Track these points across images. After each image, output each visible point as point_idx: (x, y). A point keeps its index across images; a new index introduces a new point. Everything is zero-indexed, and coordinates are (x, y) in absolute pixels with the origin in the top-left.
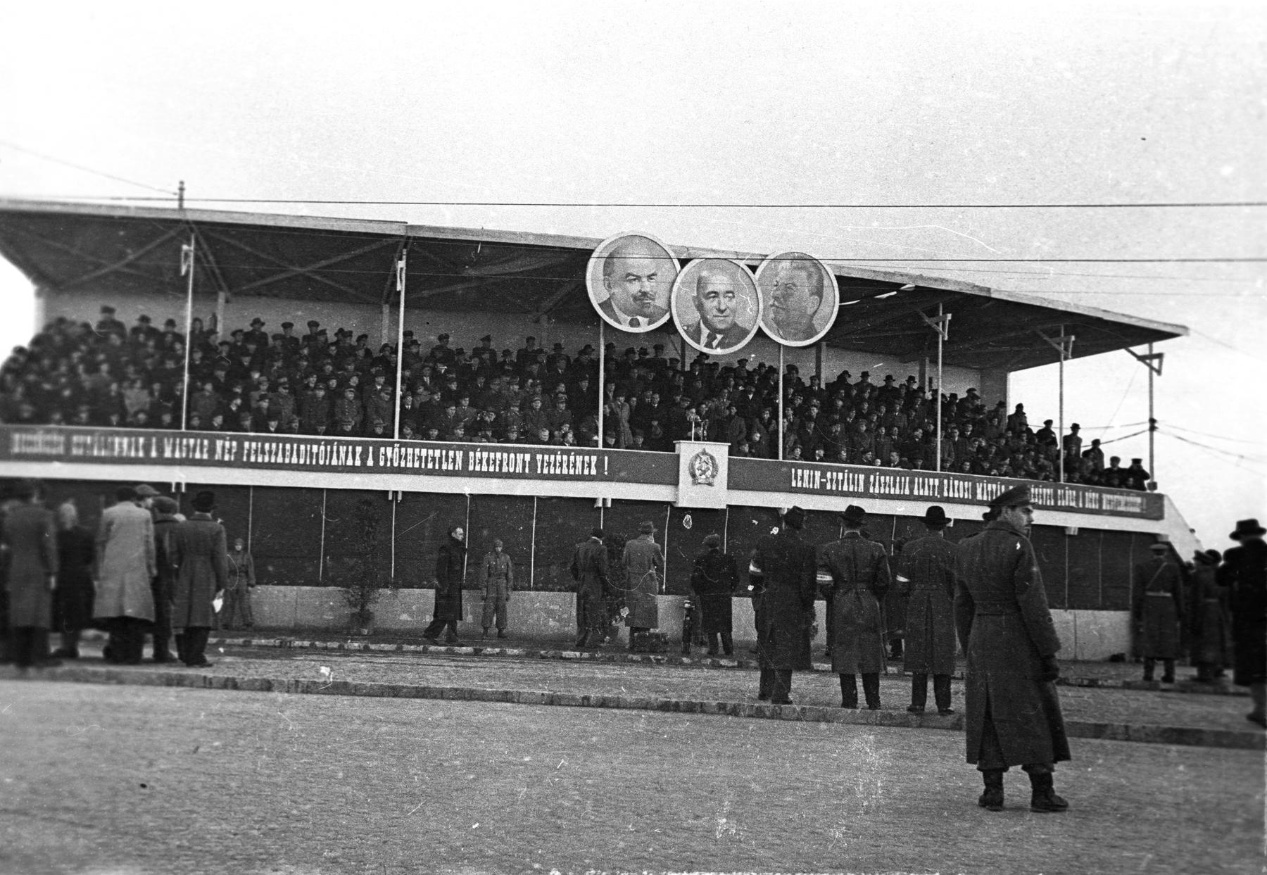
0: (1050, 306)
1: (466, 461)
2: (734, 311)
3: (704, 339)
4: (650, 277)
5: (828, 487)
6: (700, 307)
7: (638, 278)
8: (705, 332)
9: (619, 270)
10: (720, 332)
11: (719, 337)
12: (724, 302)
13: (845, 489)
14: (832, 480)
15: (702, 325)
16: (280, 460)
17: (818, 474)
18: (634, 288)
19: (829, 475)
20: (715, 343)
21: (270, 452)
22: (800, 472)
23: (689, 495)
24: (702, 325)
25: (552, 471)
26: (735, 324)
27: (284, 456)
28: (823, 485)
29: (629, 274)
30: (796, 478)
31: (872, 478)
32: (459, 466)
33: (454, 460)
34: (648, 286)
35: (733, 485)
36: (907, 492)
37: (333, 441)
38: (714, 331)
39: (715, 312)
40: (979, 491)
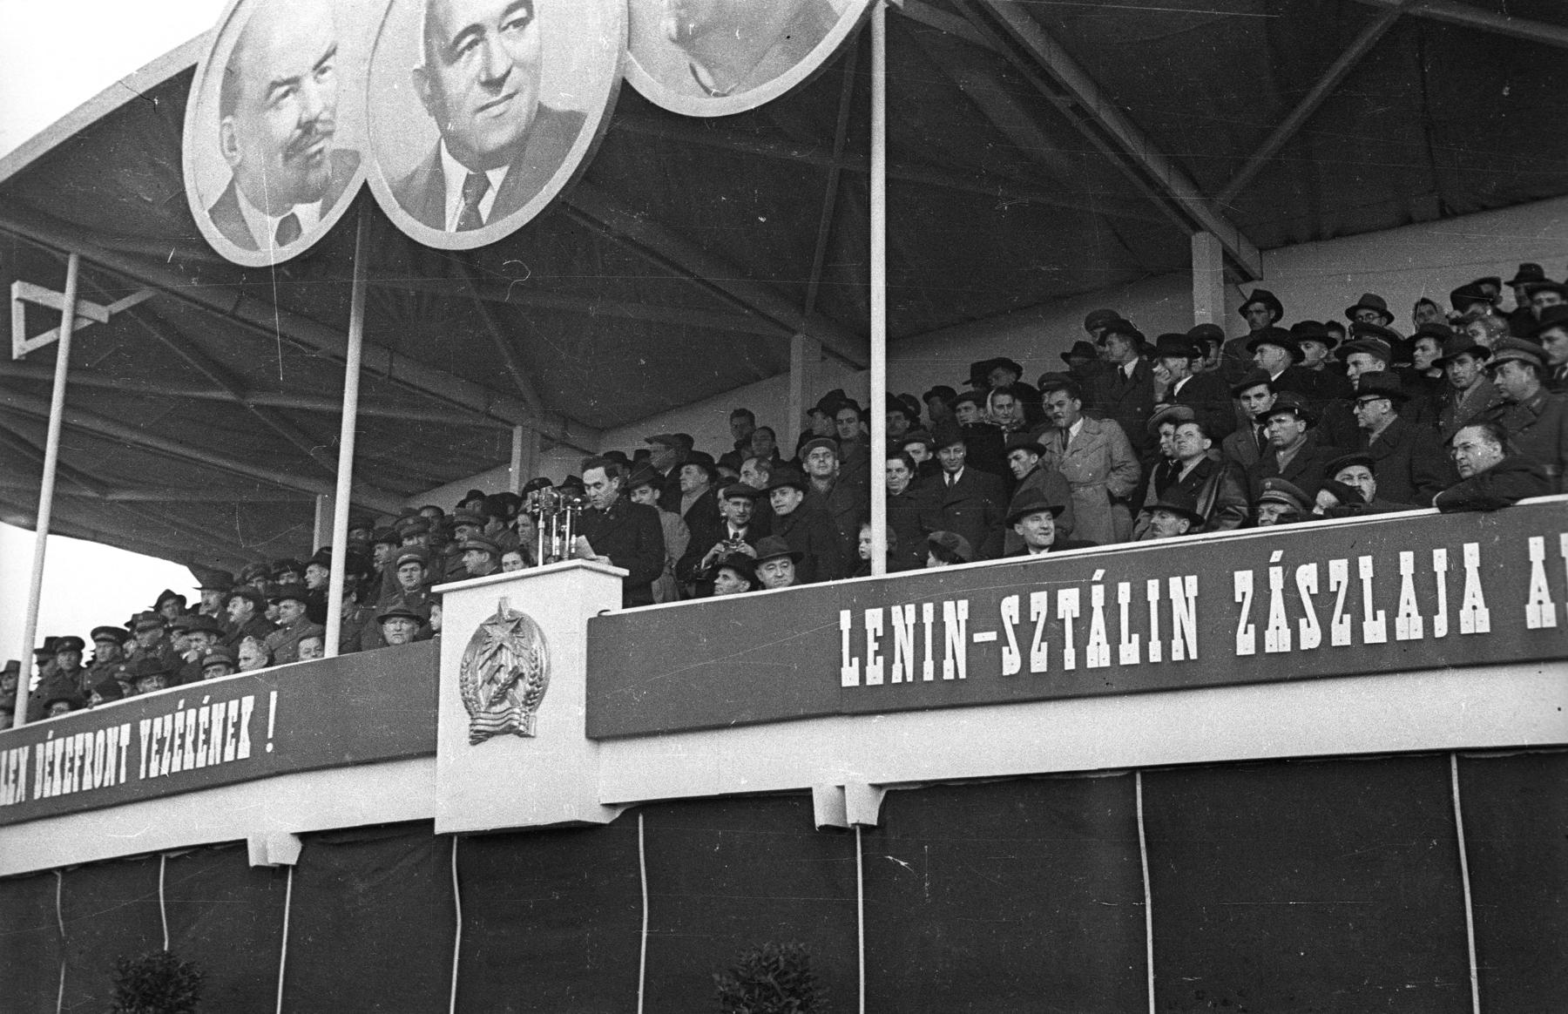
0: (75, 129)
1: (1216, 611)
2: (532, 67)
3: (455, 204)
4: (320, 68)
5: (1011, 663)
6: (438, 104)
7: (293, 84)
8: (456, 173)
9: (251, 89)
10: (493, 158)
11: (496, 176)
12: (502, 50)
13: (1098, 655)
14: (1025, 629)
15: (446, 157)
16: (1410, 627)
17: (956, 613)
18: (285, 121)
19: (1010, 607)
20: (485, 207)
21: (1324, 600)
22: (874, 618)
23: (472, 784)
24: (446, 157)
25: (1341, 634)
26: (542, 111)
27: (1427, 610)
28: (983, 658)
29: (275, 85)
30: (859, 649)
31: (1244, 581)
32: (1186, 641)
33: (886, 642)
34: (316, 96)
35: (607, 725)
36: (1476, 618)
37: (1092, 563)
38: (480, 162)
39: (482, 96)
40: (1185, 618)
